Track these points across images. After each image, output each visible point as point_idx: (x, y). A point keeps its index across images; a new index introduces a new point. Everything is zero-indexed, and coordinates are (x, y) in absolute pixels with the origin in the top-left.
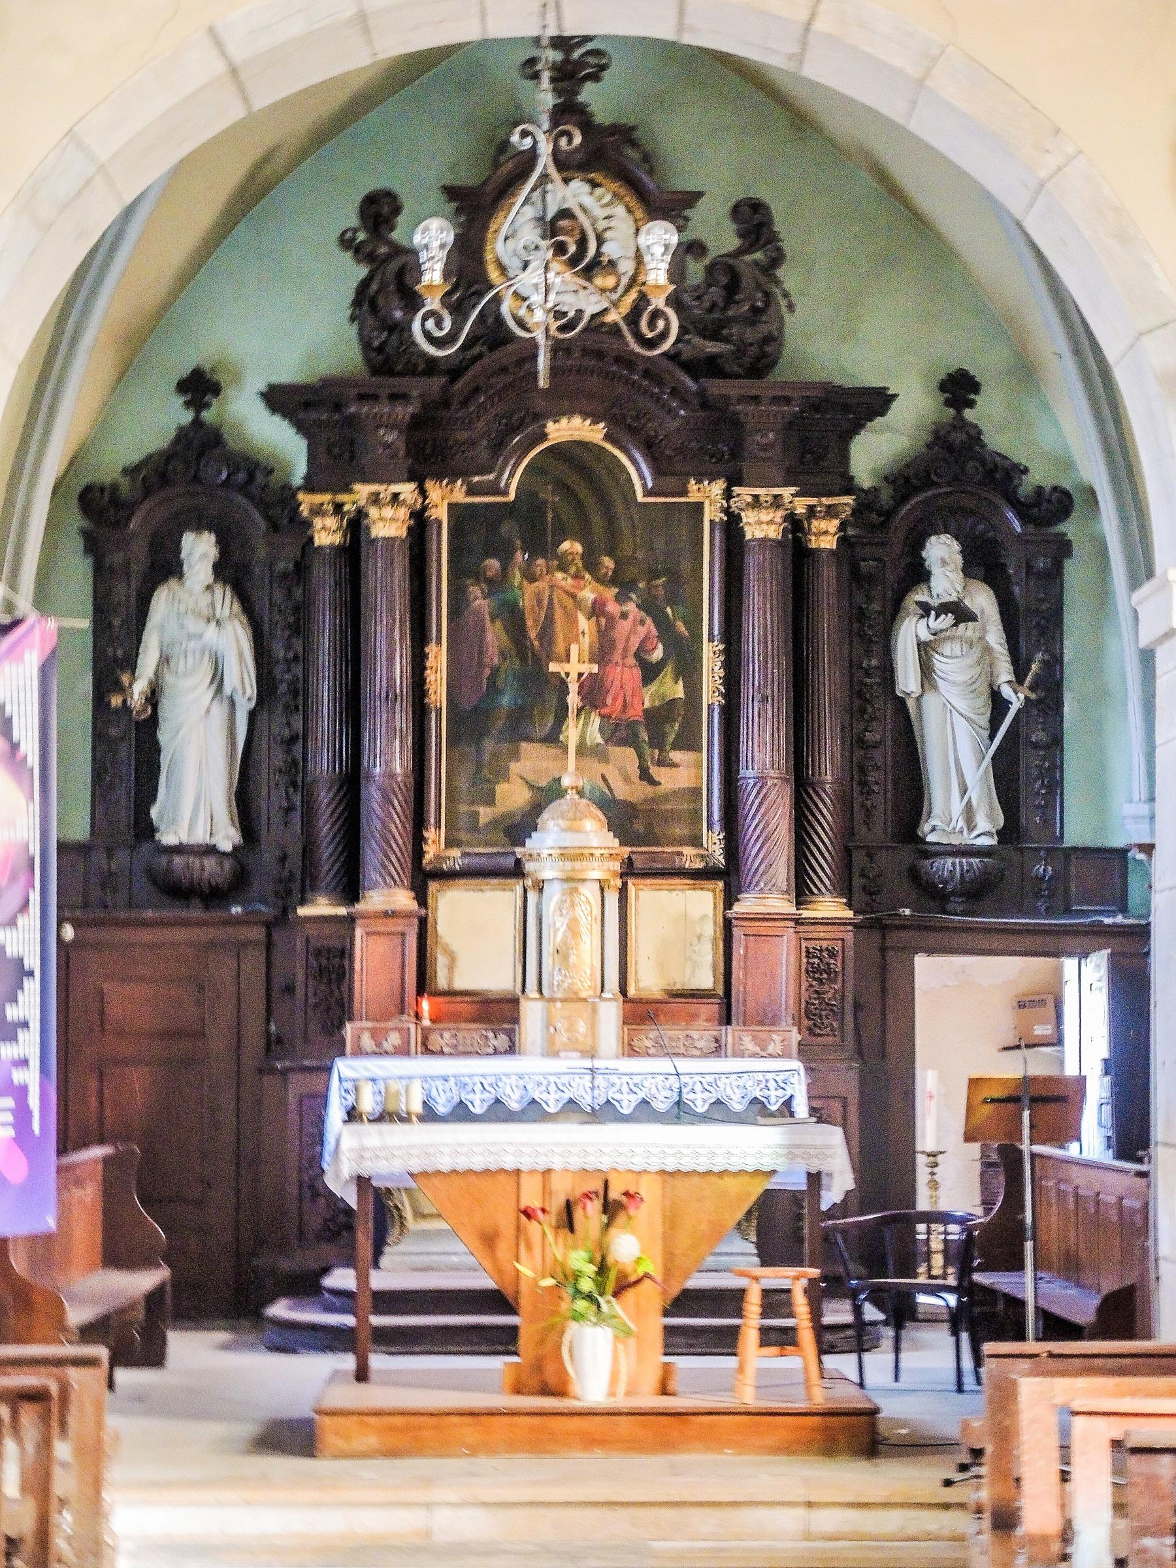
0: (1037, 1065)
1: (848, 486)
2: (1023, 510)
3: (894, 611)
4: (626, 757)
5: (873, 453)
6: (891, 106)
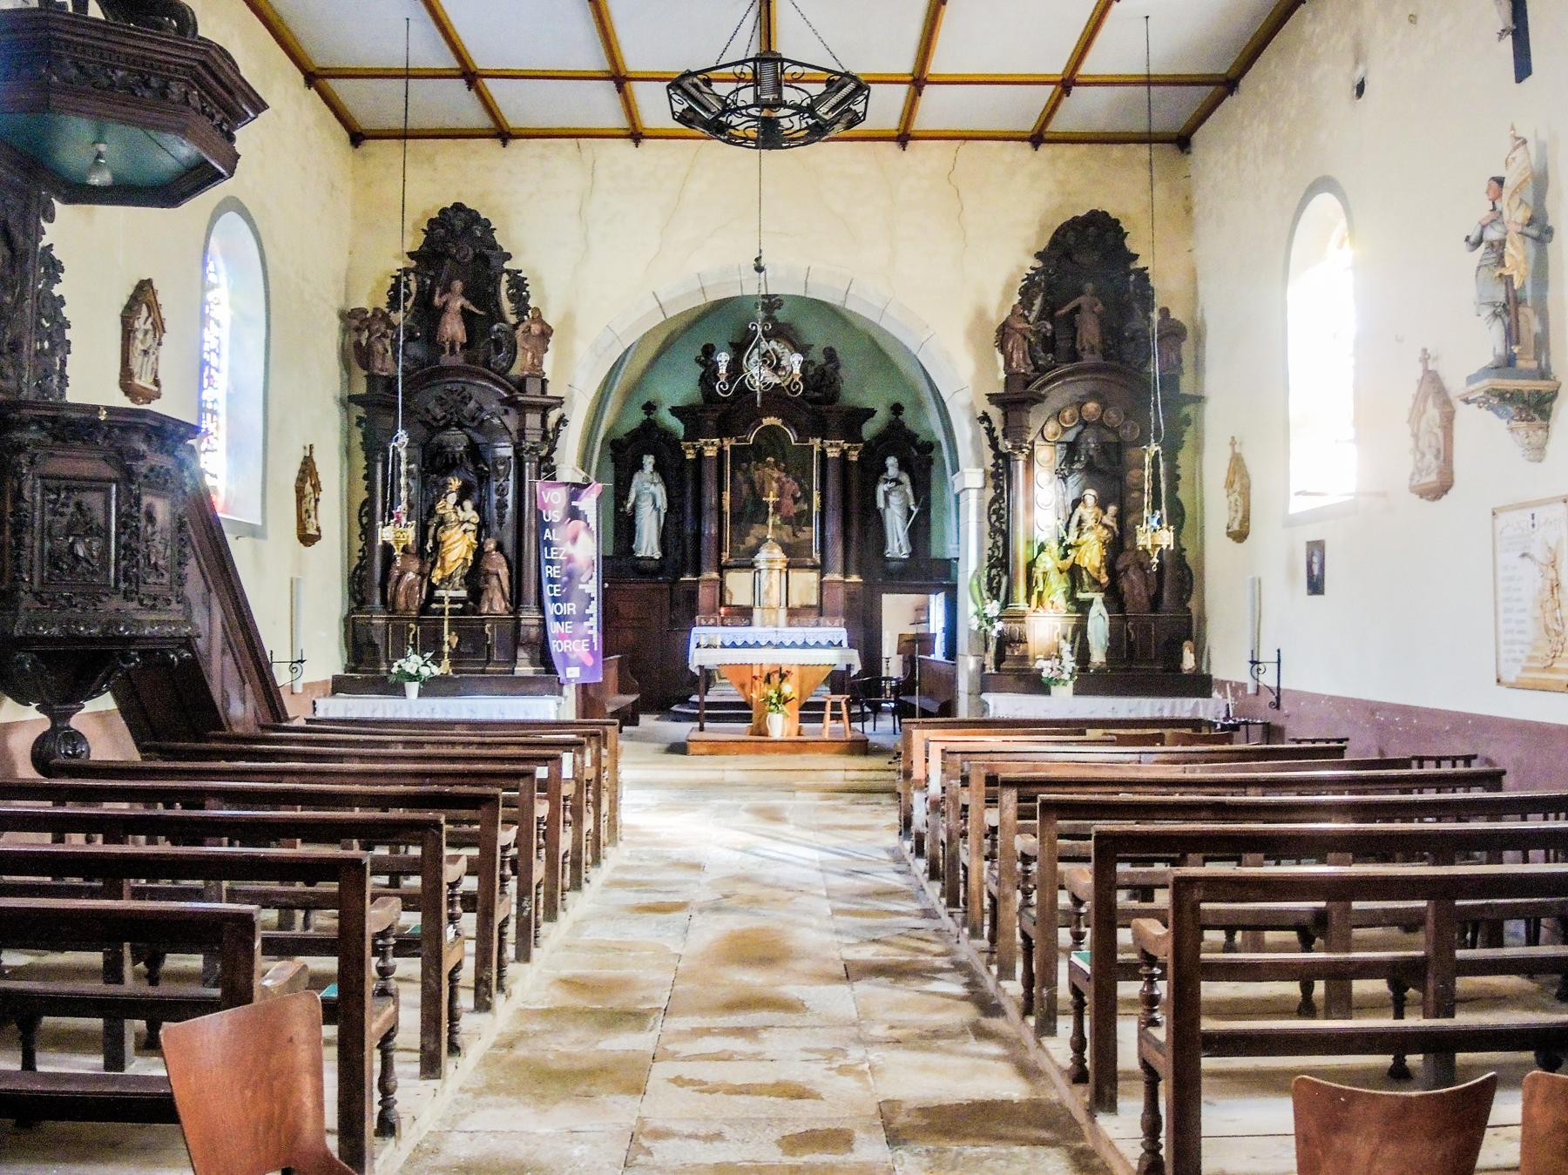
0: (921, 629)
1: (861, 441)
2: (917, 448)
3: (876, 483)
4: (788, 528)
5: (870, 429)
6: (875, 319)
